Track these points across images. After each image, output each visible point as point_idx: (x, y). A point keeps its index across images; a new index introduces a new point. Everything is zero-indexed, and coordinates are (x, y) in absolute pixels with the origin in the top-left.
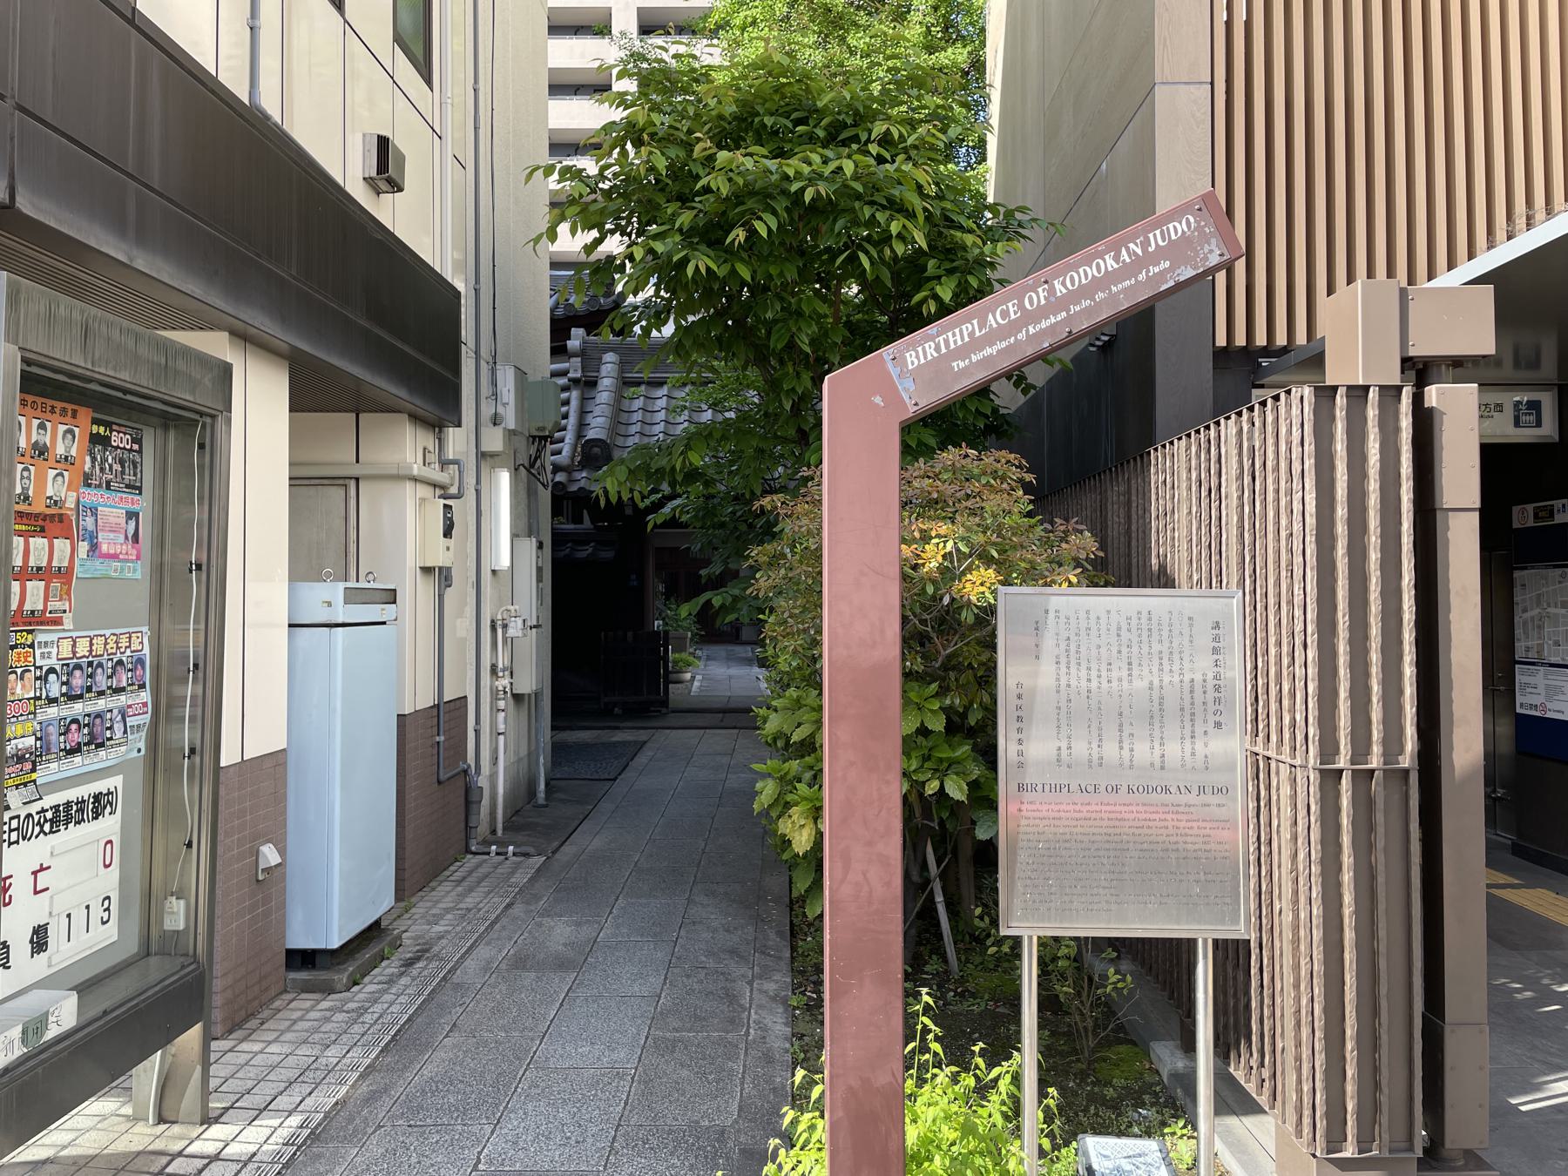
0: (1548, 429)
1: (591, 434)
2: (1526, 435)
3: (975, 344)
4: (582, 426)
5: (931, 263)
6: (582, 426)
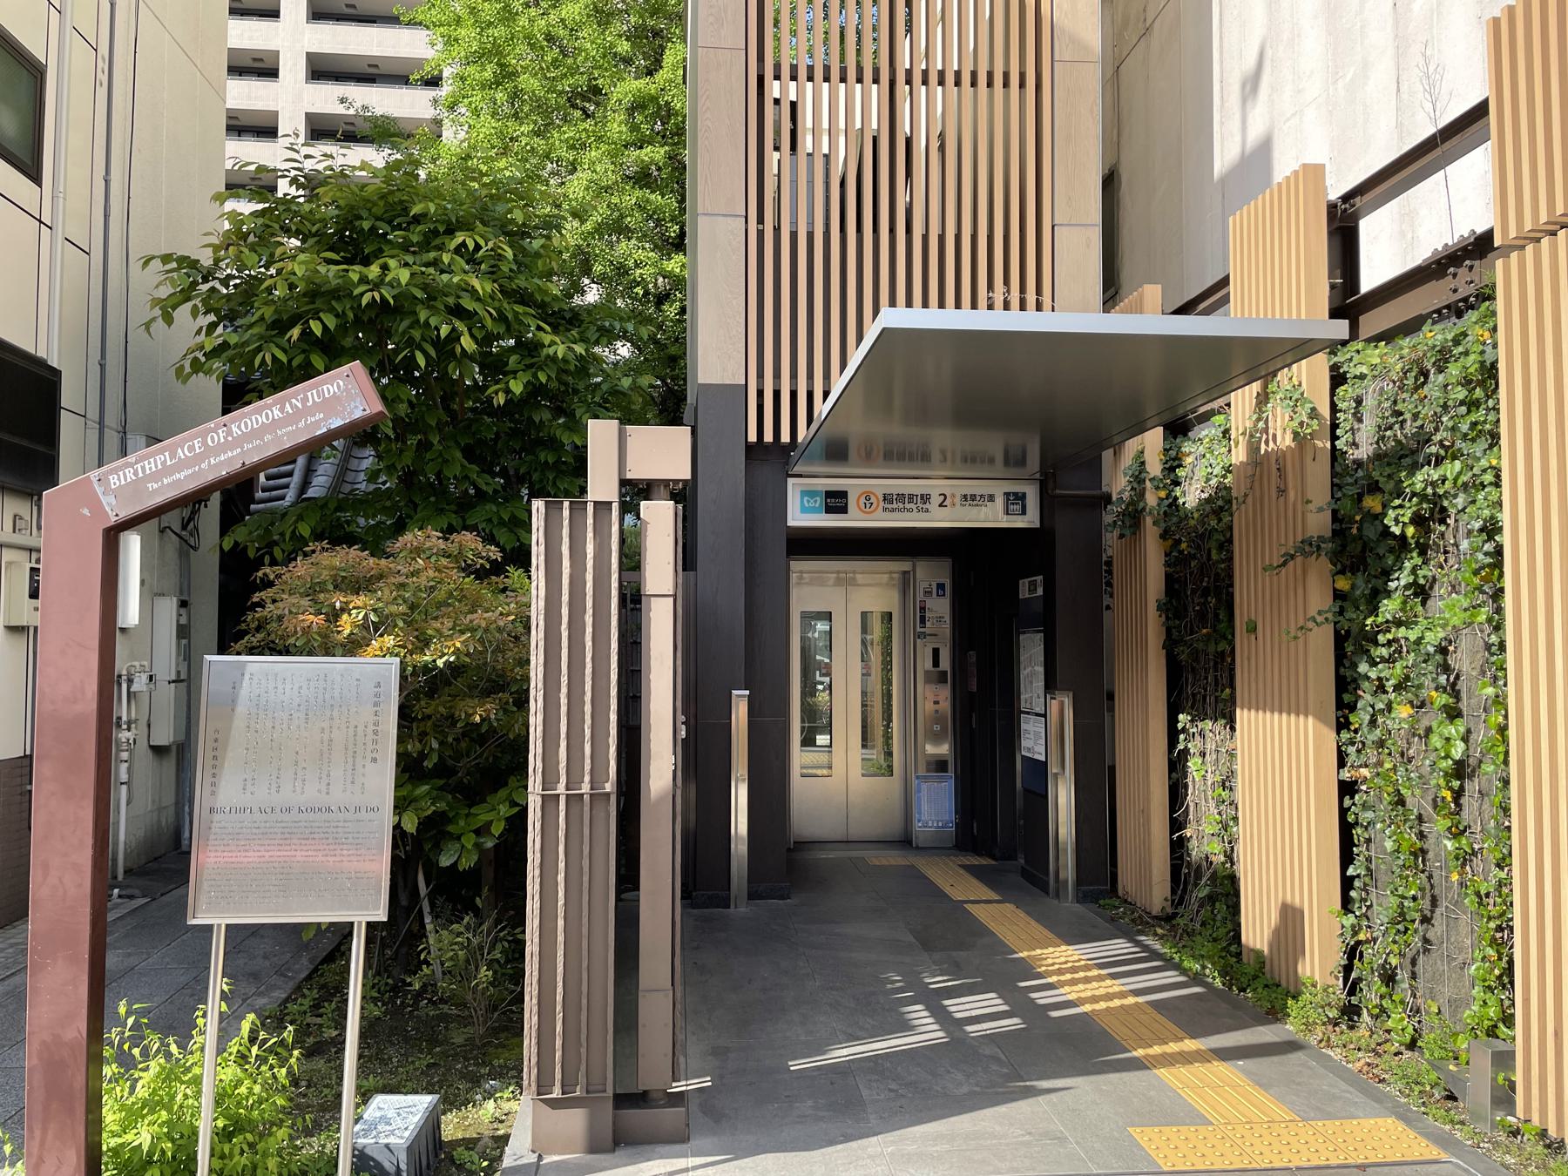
0: (1029, 519)
1: (311, 493)
2: (1019, 523)
3: (166, 471)
4: (305, 484)
5: (513, 359)
6: (305, 484)
